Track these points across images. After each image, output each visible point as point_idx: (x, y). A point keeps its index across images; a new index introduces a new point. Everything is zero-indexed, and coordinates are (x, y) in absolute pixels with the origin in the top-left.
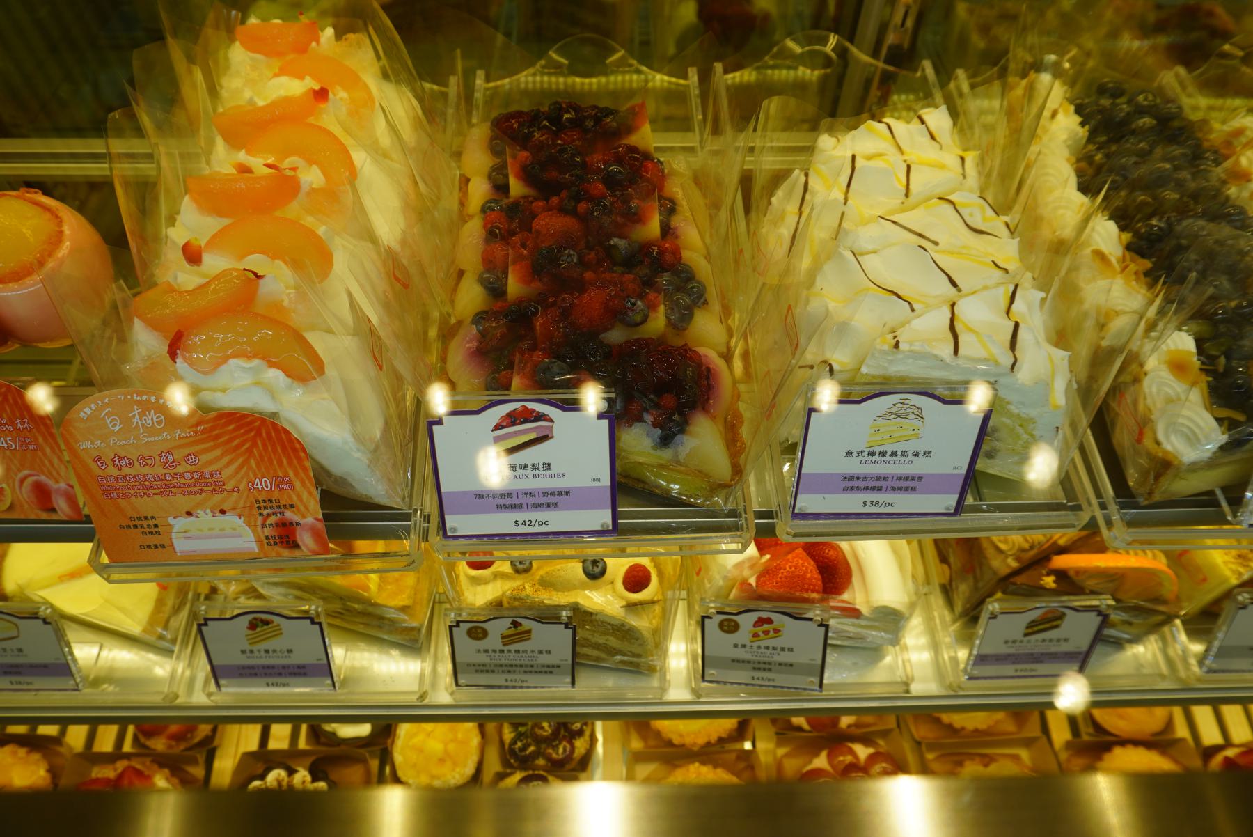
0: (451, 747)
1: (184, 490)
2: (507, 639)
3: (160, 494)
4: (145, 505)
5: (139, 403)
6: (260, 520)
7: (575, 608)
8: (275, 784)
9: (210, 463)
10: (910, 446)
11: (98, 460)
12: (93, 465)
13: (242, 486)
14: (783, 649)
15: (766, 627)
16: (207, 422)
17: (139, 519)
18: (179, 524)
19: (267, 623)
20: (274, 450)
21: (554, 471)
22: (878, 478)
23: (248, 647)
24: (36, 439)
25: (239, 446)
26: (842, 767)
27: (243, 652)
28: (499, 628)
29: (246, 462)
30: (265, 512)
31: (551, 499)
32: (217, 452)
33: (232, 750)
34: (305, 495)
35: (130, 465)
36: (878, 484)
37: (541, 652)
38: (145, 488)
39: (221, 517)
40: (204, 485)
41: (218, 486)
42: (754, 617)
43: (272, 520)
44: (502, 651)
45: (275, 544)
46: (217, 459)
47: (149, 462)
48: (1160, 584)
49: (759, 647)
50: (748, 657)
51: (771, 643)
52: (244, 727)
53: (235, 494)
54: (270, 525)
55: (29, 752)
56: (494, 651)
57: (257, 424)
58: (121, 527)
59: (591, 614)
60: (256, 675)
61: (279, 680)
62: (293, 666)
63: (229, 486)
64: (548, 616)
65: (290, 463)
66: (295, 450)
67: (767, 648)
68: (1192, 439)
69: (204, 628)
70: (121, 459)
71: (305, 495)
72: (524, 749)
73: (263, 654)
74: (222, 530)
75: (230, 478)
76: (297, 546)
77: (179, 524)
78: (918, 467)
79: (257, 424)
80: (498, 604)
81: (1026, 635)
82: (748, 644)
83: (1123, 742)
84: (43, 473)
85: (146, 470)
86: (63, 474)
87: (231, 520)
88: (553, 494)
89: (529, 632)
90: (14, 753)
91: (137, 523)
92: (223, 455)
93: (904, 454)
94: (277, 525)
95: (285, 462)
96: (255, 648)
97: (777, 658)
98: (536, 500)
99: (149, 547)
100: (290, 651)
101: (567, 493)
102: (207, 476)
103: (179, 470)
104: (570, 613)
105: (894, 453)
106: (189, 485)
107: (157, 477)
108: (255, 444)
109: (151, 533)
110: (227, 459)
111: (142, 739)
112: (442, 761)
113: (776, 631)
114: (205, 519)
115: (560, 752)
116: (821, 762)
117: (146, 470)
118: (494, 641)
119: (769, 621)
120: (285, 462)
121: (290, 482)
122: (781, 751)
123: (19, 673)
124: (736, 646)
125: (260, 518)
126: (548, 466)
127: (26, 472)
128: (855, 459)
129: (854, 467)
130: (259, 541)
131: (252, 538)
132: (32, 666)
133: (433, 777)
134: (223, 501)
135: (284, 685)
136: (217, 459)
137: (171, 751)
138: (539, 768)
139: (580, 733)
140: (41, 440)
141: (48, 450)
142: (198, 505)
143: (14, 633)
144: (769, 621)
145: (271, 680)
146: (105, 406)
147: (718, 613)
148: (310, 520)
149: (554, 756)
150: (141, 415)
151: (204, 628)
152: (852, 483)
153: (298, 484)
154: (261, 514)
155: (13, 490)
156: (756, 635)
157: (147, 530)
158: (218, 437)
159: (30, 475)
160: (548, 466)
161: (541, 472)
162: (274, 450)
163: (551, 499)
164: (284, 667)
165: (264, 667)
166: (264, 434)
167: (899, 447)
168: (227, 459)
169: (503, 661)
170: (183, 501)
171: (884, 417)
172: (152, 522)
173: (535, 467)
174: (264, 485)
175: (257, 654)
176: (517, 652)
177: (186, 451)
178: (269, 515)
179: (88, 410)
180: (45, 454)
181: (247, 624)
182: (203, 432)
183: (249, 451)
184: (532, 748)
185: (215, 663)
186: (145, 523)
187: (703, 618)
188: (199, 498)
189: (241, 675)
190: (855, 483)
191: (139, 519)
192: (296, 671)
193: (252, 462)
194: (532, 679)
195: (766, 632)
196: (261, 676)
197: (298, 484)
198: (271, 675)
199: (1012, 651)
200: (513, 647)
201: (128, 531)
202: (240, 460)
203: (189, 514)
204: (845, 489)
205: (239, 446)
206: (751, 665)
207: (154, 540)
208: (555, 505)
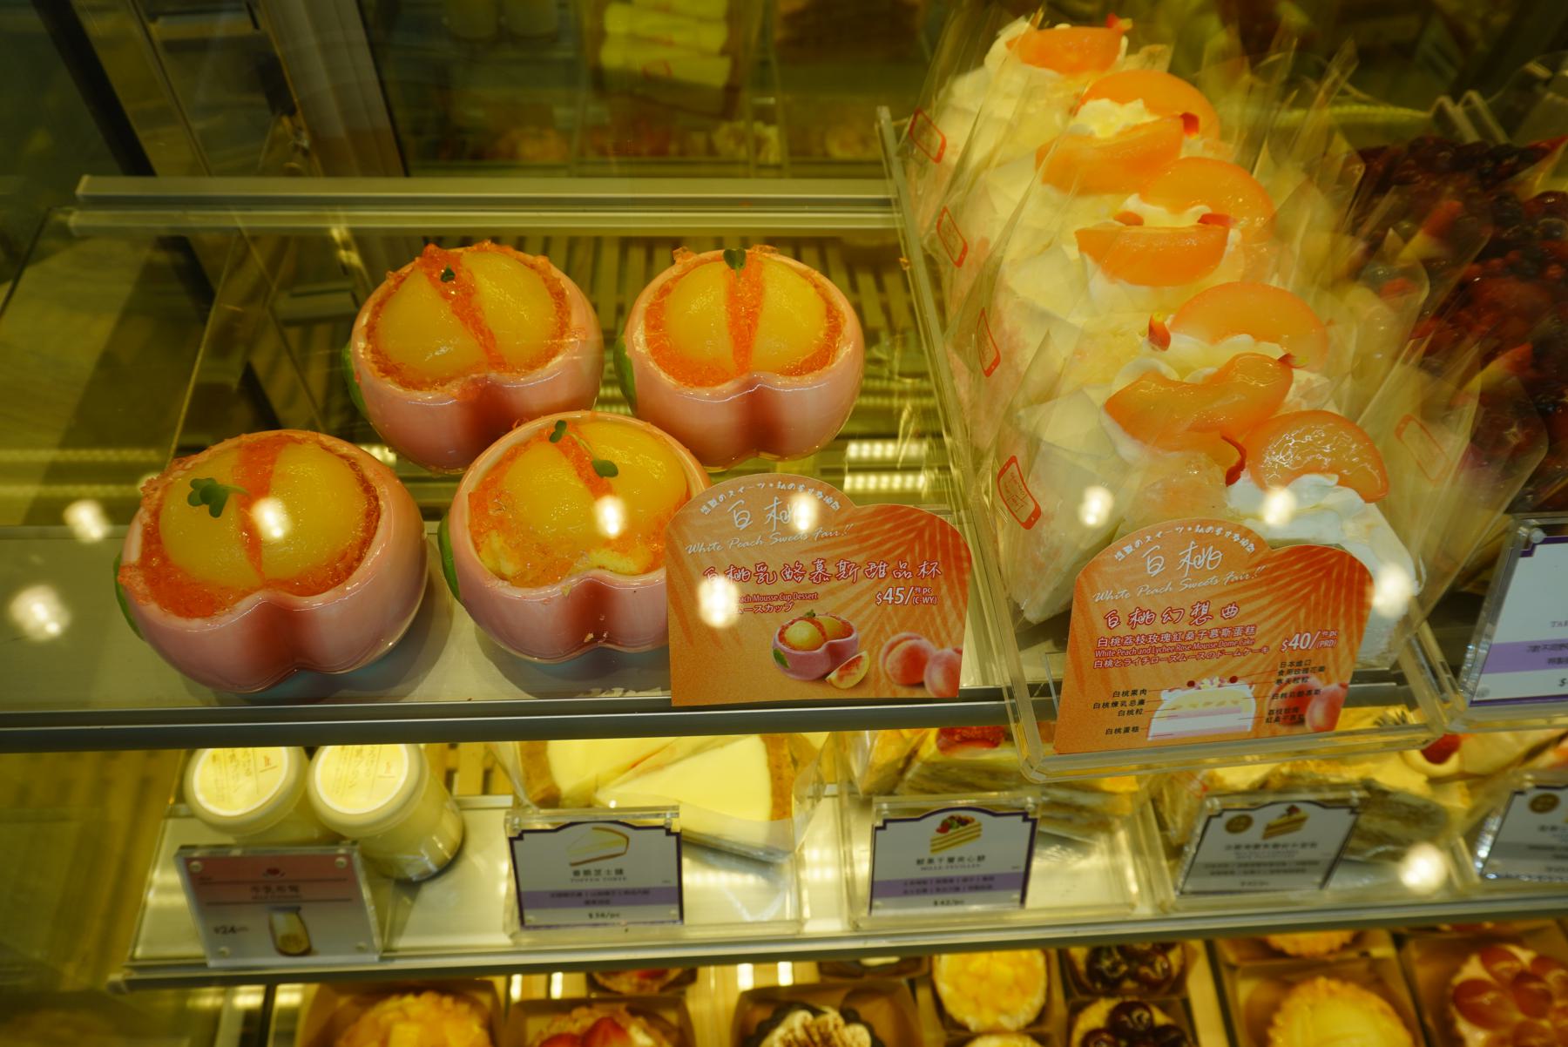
1: (1199, 652)
3: (1168, 660)
5: (1198, 537)
7: (1367, 785)
9: (1250, 615)
11: (1113, 615)
13: (1273, 646)
16: (1272, 560)
17: (1125, 693)
19: (963, 822)
23: (927, 855)
24: (939, 588)
26: (1508, 975)
30: (1285, 678)
38: (1151, 651)
43: (1291, 687)
45: (1277, 720)
47: (1175, 616)
52: (995, 954)
53: (1261, 656)
54: (1284, 695)
55: (455, 1002)
58: (1096, 706)
60: (925, 891)
61: (958, 896)
62: (978, 878)
63: (1256, 647)
69: (516, 843)
72: (1114, 968)
73: (945, 863)
74: (1222, 703)
75: (1263, 635)
80: (1263, 786)
84: (927, 634)
85: (1170, 627)
86: (954, 635)
87: (1242, 690)
90: (439, 1005)
91: (1119, 699)
92: (1284, 608)
94: (1292, 694)
95: (1342, 610)
96: (935, 856)
99: (1118, 731)
100: (981, 858)
102: (1238, 632)
103: (1209, 625)
104: (1363, 794)
106: (1209, 646)
107: (1181, 636)
108: (1316, 589)
109: (1130, 712)
111: (600, 979)
115: (654, 988)
116: (1473, 969)
120: (1342, 610)
121: (1335, 638)
123: (607, 903)
125: (1276, 686)
127: (904, 634)
131: (1252, 713)
135: (957, 903)
136: (1263, 608)
137: (645, 993)
138: (1129, 992)
140: (944, 589)
141: (948, 603)
142: (1208, 673)
143: (621, 849)
145: (939, 897)
147: (1538, 787)
149: (1153, 975)
150: (1197, 552)
151: (516, 843)
154: (1279, 681)
155: (874, 661)
157: (1125, 709)
159: (907, 639)
164: (965, 879)
165: (939, 881)
166: (1334, 575)
170: (1191, 667)
172: (1138, 698)
174: (1301, 642)
175: (936, 863)
176: (1276, 846)
177: (1230, 599)
178: (1289, 681)
179: (1128, 549)
180: (941, 609)
182: (1261, 574)
183: (1306, 597)
184: (1124, 968)
185: (523, 889)
186: (1128, 699)
188: (1214, 661)
189: (906, 893)
191: (1125, 693)
192: (981, 883)
193: (1302, 614)
194: (1275, 881)
196: (932, 892)
198: (945, 891)
201: (1101, 711)
202: (1289, 610)
203: (1191, 684)
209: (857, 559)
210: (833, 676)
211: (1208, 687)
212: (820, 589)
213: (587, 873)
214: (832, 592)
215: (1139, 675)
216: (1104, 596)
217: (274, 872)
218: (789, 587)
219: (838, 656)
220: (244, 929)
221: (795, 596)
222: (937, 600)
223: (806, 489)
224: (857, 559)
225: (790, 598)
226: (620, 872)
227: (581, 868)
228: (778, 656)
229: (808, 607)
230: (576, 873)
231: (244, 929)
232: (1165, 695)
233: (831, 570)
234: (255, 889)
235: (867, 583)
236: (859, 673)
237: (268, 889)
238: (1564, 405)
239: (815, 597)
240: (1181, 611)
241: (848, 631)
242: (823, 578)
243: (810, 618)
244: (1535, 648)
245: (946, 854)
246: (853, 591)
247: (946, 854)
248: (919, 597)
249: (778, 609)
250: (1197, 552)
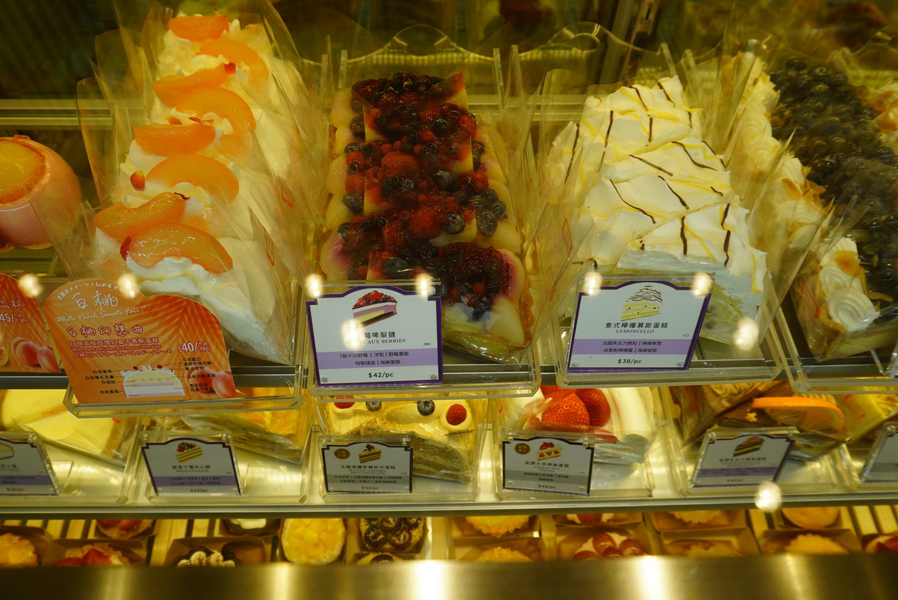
0: (324, 535)
1: (132, 351)
2: (363, 458)
3: (115, 354)
4: (104, 362)
5: (100, 289)
6: (186, 373)
7: (412, 436)
8: (197, 562)
9: (151, 332)
10: (652, 320)
11: (70, 329)
12: (66, 334)
13: (173, 349)
14: (561, 465)
15: (549, 449)
16: (149, 302)
17: (100, 372)
18: (128, 376)
19: (191, 446)
20: (197, 323)
21: (397, 337)
22: (629, 343)
23: (177, 464)
24: (26, 315)
25: (171, 320)
26: (603, 550)
27: (174, 467)
28: (358, 450)
29: (176, 331)
30: (190, 367)
31: (395, 358)
32: (156, 324)
33: (166, 538)
34: (218, 355)
35: (93, 333)
36: (629, 347)
37: (387, 467)
38: (104, 350)
39: (158, 371)
40: (146, 348)
41: (156, 348)
42: (540, 442)
43: (195, 372)
44: (360, 467)
45: (197, 390)
46: (156, 329)
47: (107, 331)
48: (832, 419)
49: (544, 464)
50: (536, 471)
51: (553, 461)
52: (175, 521)
53: (168, 354)
54: (194, 376)
55: (21, 539)
56: (354, 467)
57: (184, 304)
58: (87, 378)
59: (424, 440)
60: (183, 484)
61: (200, 487)
62: (210, 477)
63: (164, 349)
64: (393, 441)
65: (208, 332)
66: (211, 323)
67: (550, 464)
68: (854, 315)
69: (146, 450)
70: (87, 329)
71: (218, 355)
72: (375, 537)
73: (188, 468)
74: (159, 380)
75: (165, 343)
76: (213, 392)
77: (128, 376)
78: (658, 334)
79: (184, 304)
80: (357, 433)
81: (735, 455)
82: (536, 462)
83: (805, 532)
84: (31, 339)
85: (104, 337)
86: (45, 340)
87: (166, 373)
88: (396, 354)
89: (379, 453)
90: (10, 540)
91: (98, 375)
92: (160, 326)
93: (648, 325)
94: (199, 376)
95: (204, 331)
96: (183, 464)
97: (557, 472)
98: (384, 359)
99: (107, 392)
100: (208, 467)
101: (406, 354)
102: (149, 341)
103: (128, 337)
104: (408, 440)
105: (641, 325)
106: (135, 348)
107: (112, 342)
108: (182, 319)
109: (108, 382)
110: (163, 329)
111: (102, 530)
112: (316, 545)
113: (556, 452)
114: (147, 372)
115: (401, 539)
116: (588, 546)
117: (104, 337)
118: (354, 460)
119: (551, 445)
120: (204, 331)
121: (208, 346)
122: (560, 539)
123: (13, 483)
124: (527, 463)
125: (186, 372)
126: (392, 334)
127: (19, 338)
128: (613, 329)
129: (612, 334)
130: (186, 388)
131: (181, 386)
132: (23, 478)
133: (310, 557)
134: (160, 359)
135: (204, 491)
136: (156, 329)
137: (122, 539)
138: (386, 550)
139: (416, 525)
140: (29, 315)
141: (34, 323)
142: (142, 362)
143: (10, 454)
144: (551, 445)
145: (194, 488)
146: (75, 291)
147: (515, 439)
148: (222, 373)
149: (397, 542)
150: (101, 297)
151: (146, 450)
152: (611, 347)
153: (213, 347)
154: (187, 369)
155: (9, 352)
156: (542, 455)
157: (106, 380)
158: (156, 313)
159: (22, 341)
160: (392, 334)
161: (388, 338)
162: (197, 323)
163: (395, 358)
164: (203, 478)
165: (189, 478)
166: (189, 311)
167: (645, 321)
168: (163, 329)
169: (360, 474)
170: (131, 359)
171: (633, 299)
172: (109, 374)
173: (383, 335)
174: (189, 348)
175: (184, 469)
176: (371, 467)
177: (133, 323)
178: (193, 369)
179: (63, 294)
180: (32, 326)
181: (177, 447)
182: (145, 310)
183: (179, 323)
184: (381, 536)
185: (154, 475)
186: (104, 375)
187: (504, 443)
188: (142, 357)
189: (173, 484)
190: (613, 347)
191: (100, 372)
192: (212, 481)
193: (181, 331)
194: (382, 487)
195: (549, 453)
196: (187, 484)
197: (213, 347)
198: (194, 484)
199: (725, 467)
200: (368, 464)
201: (92, 381)
202: (172, 330)
203: (135, 368)
204: (606, 351)
205: (171, 320)
206: (538, 477)
207: (111, 387)
208: (398, 362)
223: (436, 287)
238: (894, 257)
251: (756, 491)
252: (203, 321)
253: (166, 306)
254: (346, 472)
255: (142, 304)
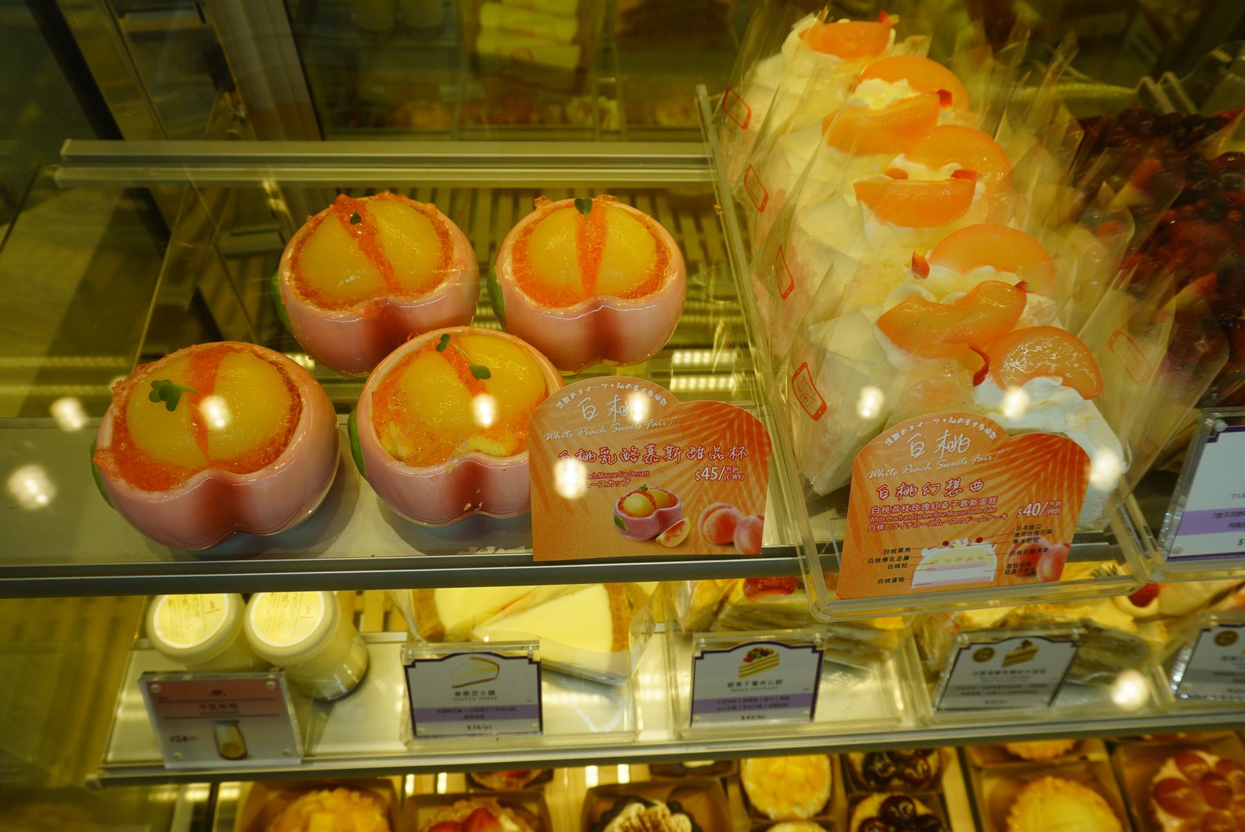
1: (952, 518)
3: (928, 524)
5: (952, 427)
7: (1086, 623)
9: (993, 488)
11: (884, 489)
13: (1011, 513)
16: (1010, 445)
17: (893, 551)
19: (765, 653)
23: (736, 679)
24: (745, 468)
26: (1197, 775)
30: (1020, 539)
38: (914, 518)
43: (1025, 546)
45: (1014, 572)
47: (933, 490)
52: (790, 758)
53: (1001, 521)
54: (1019, 553)
55: (362, 796)
57: (733, 415)
58: (871, 561)
60: (734, 708)
61: (760, 712)
62: (776, 698)
63: (997, 514)
66: (761, 444)
72: (885, 769)
73: (750, 686)
74: (970, 559)
75: (1003, 504)
79: (733, 415)
80: (1003, 625)
84: (736, 504)
85: (929, 499)
86: (758, 505)
87: (986, 548)
90: (348, 798)
91: (888, 556)
92: (1020, 483)
94: (1026, 552)
95: (1066, 485)
96: (743, 680)
99: (888, 581)
100: (779, 682)
102: (983, 502)
103: (960, 497)
104: (1082, 631)
106: (960, 513)
107: (938, 505)
108: (1045, 468)
109: (897, 566)
111: (477, 778)
116: (1170, 770)
120: (1066, 485)
121: (1060, 507)
123: (482, 717)
125: (1013, 545)
127: (717, 504)
131: (994, 567)
135: (760, 717)
136: (1003, 483)
137: (512, 789)
138: (896, 788)
140: (750, 468)
141: (753, 479)
142: (959, 535)
143: (493, 674)
145: (746, 713)
147: (1221, 626)
149: (915, 775)
150: (950, 438)
154: (1016, 541)
155: (694, 525)
157: (893, 563)
159: (720, 507)
164: (766, 699)
165: (745, 700)
166: (1059, 457)
170: (945, 530)
172: (903, 555)
174: (1033, 510)
175: (744, 686)
176: (1013, 672)
177: (977, 476)
178: (1023, 542)
179: (896, 437)
180: (747, 484)
182: (1001, 456)
183: (1037, 475)
184: (892, 769)
186: (896, 556)
188: (964, 525)
189: (719, 709)
191: (893, 551)
192: (779, 702)
193: (1034, 488)
194: (1012, 700)
196: (740, 709)
198: (750, 708)
201: (874, 565)
202: (1024, 485)
203: (946, 544)
209: (681, 444)
210: (661, 537)
211: (959, 546)
212: (651, 468)
213: (466, 693)
214: (660, 471)
215: (905, 536)
216: (876, 473)
217: (217, 693)
218: (627, 466)
219: (666, 521)
220: (194, 738)
221: (631, 473)
222: (744, 477)
224: (681, 444)
225: (627, 476)
226: (492, 693)
227: (462, 690)
228: (618, 521)
229: (642, 482)
230: (458, 694)
231: (194, 738)
232: (925, 552)
233: (660, 453)
234: (203, 706)
235: (688, 463)
236: (682, 535)
237: (213, 707)
239: (647, 474)
240: (938, 485)
241: (673, 501)
242: (654, 459)
243: (643, 491)
244: (1219, 515)
245: (751, 678)
246: (677, 469)
247: (751, 678)
248: (730, 475)
249: (617, 484)
250: (950, 438)
251: (543, 789)
252: (751, 440)
253: (705, 418)
254: (1228, 666)
255: (673, 414)
